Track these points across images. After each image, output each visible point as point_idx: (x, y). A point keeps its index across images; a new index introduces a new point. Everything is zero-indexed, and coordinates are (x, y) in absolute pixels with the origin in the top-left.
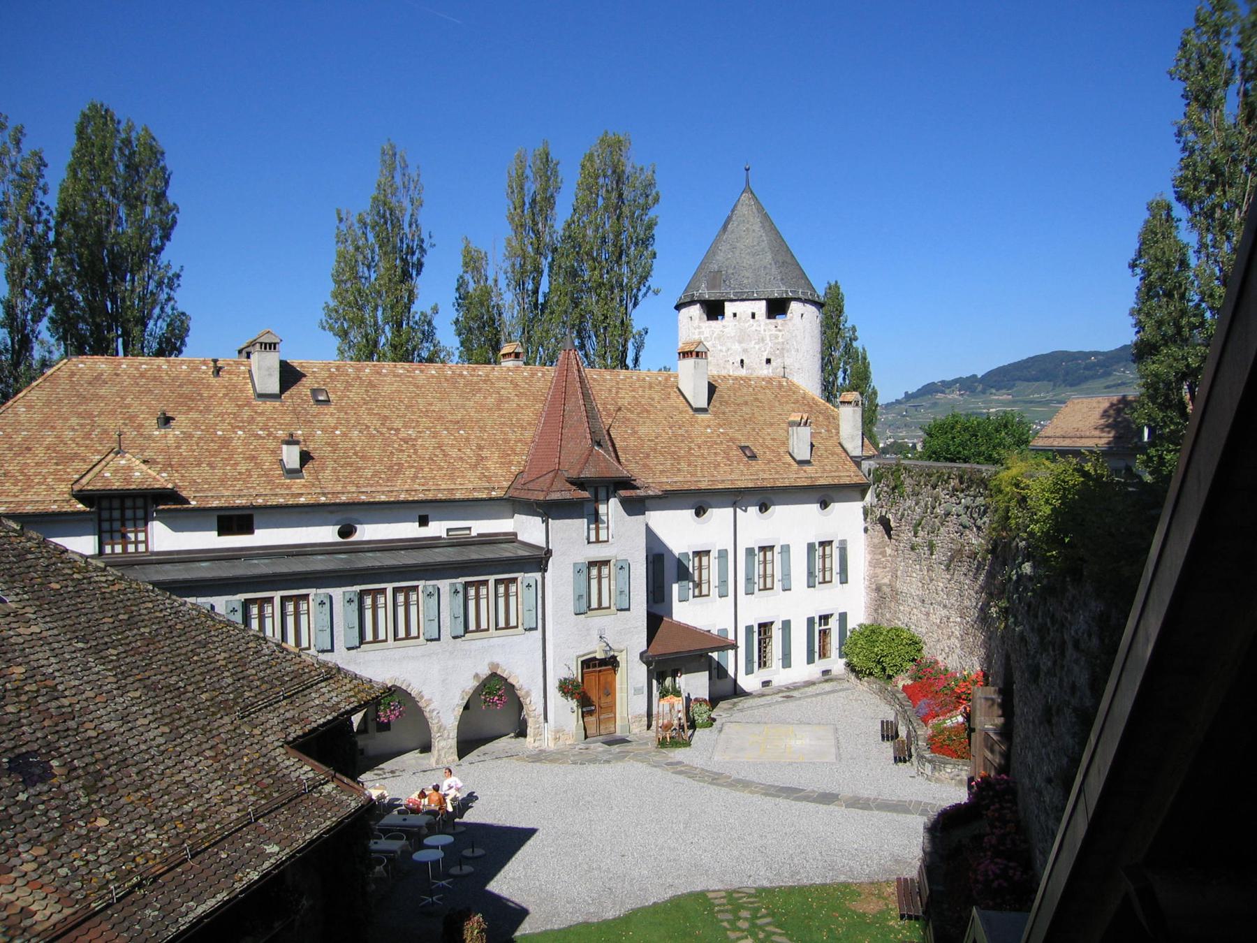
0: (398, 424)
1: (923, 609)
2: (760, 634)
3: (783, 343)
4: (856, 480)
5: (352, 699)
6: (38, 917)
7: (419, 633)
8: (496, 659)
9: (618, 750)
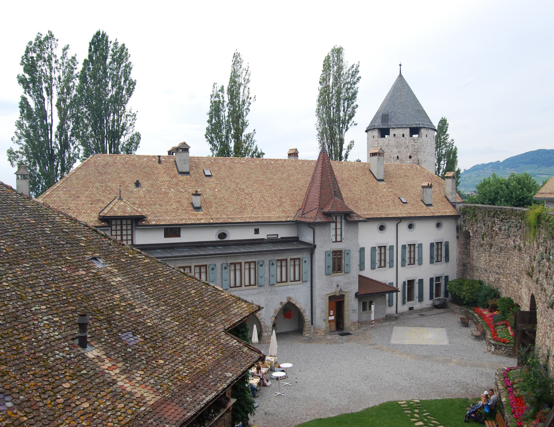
0: (243, 186)
1: (486, 275)
2: (408, 286)
3: (417, 148)
4: (453, 214)
5: (247, 312)
6: (147, 399)
7: (255, 283)
8: (290, 295)
9: (345, 338)
